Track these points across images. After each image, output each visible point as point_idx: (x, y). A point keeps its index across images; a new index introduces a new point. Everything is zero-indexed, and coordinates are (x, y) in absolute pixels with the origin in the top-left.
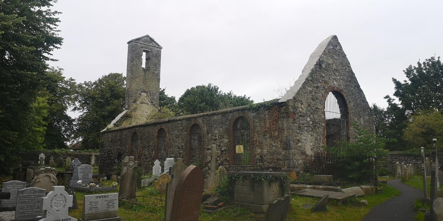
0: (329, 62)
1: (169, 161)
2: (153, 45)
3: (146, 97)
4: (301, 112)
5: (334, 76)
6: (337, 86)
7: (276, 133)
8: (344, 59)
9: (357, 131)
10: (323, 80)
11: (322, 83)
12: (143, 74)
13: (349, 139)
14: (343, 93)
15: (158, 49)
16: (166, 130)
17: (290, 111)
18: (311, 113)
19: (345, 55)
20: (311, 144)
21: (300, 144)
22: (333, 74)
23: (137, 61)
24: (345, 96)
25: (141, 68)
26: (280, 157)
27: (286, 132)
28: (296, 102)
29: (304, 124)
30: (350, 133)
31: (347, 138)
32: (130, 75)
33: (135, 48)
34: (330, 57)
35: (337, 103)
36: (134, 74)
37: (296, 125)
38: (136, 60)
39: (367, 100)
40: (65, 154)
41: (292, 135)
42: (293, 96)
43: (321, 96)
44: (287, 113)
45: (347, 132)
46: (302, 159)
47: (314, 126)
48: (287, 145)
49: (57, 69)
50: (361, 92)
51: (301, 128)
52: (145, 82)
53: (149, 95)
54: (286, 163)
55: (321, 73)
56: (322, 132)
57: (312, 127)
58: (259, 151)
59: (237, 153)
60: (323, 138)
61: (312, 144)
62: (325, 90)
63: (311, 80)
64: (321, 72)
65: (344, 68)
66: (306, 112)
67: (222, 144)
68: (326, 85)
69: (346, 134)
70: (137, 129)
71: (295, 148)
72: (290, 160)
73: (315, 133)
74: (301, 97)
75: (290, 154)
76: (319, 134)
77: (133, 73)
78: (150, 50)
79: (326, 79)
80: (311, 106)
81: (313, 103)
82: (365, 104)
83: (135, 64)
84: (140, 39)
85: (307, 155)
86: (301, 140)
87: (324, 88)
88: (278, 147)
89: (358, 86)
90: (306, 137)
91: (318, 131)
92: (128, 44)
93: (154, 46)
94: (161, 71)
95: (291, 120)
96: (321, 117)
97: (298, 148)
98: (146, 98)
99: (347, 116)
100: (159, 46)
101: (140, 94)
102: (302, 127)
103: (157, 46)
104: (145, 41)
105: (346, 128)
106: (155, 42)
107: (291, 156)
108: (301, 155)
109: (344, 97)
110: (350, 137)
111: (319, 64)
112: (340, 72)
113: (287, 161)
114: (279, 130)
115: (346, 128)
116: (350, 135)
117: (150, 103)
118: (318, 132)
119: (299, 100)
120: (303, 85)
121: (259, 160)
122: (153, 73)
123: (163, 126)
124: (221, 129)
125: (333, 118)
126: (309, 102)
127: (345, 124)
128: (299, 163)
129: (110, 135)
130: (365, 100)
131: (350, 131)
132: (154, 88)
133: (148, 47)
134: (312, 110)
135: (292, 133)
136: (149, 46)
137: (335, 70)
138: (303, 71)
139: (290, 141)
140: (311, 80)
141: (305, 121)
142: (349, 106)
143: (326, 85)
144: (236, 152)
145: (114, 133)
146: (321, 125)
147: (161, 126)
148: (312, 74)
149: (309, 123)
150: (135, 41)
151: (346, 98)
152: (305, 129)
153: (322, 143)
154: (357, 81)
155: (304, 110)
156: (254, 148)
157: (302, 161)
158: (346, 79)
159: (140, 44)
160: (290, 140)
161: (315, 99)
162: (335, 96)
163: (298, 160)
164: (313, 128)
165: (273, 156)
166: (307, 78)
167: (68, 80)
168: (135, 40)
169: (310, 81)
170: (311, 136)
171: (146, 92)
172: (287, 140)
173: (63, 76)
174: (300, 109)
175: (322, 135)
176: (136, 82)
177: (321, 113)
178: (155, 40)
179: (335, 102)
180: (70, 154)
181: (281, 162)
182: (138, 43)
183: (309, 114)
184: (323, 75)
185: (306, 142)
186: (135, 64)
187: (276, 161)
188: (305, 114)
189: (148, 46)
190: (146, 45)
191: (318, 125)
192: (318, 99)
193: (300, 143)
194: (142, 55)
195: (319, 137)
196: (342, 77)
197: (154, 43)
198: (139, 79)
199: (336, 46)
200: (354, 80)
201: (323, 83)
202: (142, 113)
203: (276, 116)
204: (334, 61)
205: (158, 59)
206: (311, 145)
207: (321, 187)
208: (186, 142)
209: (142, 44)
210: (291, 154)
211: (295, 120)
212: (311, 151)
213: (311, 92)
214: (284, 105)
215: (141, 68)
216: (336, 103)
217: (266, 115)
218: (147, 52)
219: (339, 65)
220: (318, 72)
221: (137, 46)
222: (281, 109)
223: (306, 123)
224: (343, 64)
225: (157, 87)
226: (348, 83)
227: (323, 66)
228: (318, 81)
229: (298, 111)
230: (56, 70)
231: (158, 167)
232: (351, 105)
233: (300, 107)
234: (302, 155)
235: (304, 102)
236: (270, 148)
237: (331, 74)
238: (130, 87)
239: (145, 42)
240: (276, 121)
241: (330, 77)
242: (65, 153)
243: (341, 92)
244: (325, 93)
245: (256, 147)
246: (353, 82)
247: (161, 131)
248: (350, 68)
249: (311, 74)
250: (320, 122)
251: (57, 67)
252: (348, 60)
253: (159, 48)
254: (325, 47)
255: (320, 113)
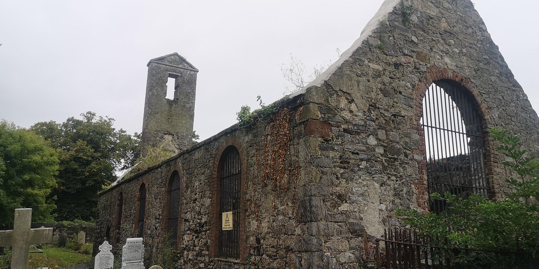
0: (428, 11)
1: (131, 244)
2: (184, 67)
3: (172, 141)
4: (347, 122)
5: (443, 45)
6: (453, 68)
7: (285, 180)
8: (470, 11)
9: (510, 160)
10: (414, 52)
11: (409, 56)
12: (167, 108)
13: (495, 196)
14: (469, 86)
17: (315, 117)
18: (380, 126)
19: (471, 3)
20: (380, 208)
21: (344, 207)
22: (442, 41)
23: (159, 89)
24: (475, 92)
25: (164, 100)
26: (292, 243)
27: (303, 172)
28: (331, 95)
29: (358, 154)
30: (495, 182)
31: (488, 192)
32: (148, 109)
33: (156, 72)
34: (432, 3)
35: (455, 109)
36: (154, 108)
37: (331, 154)
38: (157, 88)
39: (534, 108)
40: (78, 227)
41: (318, 181)
42: (323, 79)
43: (410, 86)
44: (306, 122)
45: (488, 180)
46: (351, 248)
47: (390, 158)
48: (305, 209)
49: (106, 119)
50: (518, 89)
51: (348, 163)
52: (170, 120)
53: (176, 138)
54: (303, 262)
55: (406, 34)
56: (414, 176)
57: (384, 161)
58: (254, 224)
59: (223, 230)
60: (419, 192)
61: (383, 207)
62: (419, 75)
63: (379, 48)
64: (407, 32)
65: (470, 30)
66: (365, 122)
68: (422, 63)
69: (485, 185)
71: (329, 217)
72: (312, 252)
73: (393, 178)
74: (349, 83)
75: (312, 235)
76: (404, 180)
77: (151, 107)
78: (179, 74)
79: (424, 48)
80: (379, 108)
81: (385, 101)
82: (530, 117)
83: (156, 93)
84: (163, 58)
85: (369, 238)
86: (350, 194)
87: (418, 69)
88: (288, 214)
89: (509, 75)
90: (366, 188)
91: (401, 174)
92: (148, 67)
93: (185, 68)
94: (195, 104)
95: (316, 141)
96: (409, 137)
97: (340, 218)
98: (171, 143)
99: (484, 142)
100: (194, 68)
101: (162, 138)
102: (352, 161)
103: (190, 68)
104: (172, 62)
105: (483, 171)
106: (188, 63)
107: (315, 241)
108: (347, 238)
109: (473, 96)
110: (497, 190)
112: (459, 37)
113: (305, 256)
114: (290, 171)
115: (483, 171)
116: (496, 186)
118: (401, 176)
119: (340, 90)
120: (353, 55)
121: (254, 248)
122: (183, 106)
125: (456, 155)
126: (372, 99)
127: (482, 160)
128: (342, 260)
130: (529, 107)
131: (495, 177)
132: (183, 128)
133: (176, 69)
134: (382, 118)
135: (319, 176)
136: (179, 69)
137: (445, 31)
139: (313, 198)
140: (379, 48)
141: (360, 145)
142: (487, 117)
143: (422, 63)
144: (223, 226)
146: (412, 159)
148: (381, 32)
149: (374, 151)
150: (155, 61)
151: (479, 99)
152: (361, 167)
153: (416, 204)
154: (505, 62)
155: (356, 116)
156: (246, 217)
157: (351, 255)
158: (475, 55)
159: (164, 66)
160: (312, 196)
161: (392, 91)
162: (446, 91)
163: (340, 252)
164: (386, 164)
165: (279, 239)
166: (367, 41)
167: (118, 132)
168: (156, 60)
169: (375, 48)
170: (381, 186)
171: (171, 134)
172: (305, 195)
173: (112, 127)
174: (346, 115)
175: (415, 184)
176: (156, 119)
177: (408, 126)
178: (188, 60)
179: (451, 107)
180: (85, 228)
181: (293, 256)
182: (161, 64)
183: (374, 129)
184: (414, 39)
185: (365, 202)
186: (156, 93)
187: (282, 252)
188: (361, 128)
189: (176, 68)
190: (174, 68)
191: (402, 157)
192: (400, 93)
193: (346, 205)
194: (166, 81)
195: (405, 190)
196: (464, 50)
197: (186, 64)
198: (161, 115)
200: (496, 61)
201: (415, 57)
203: (285, 135)
204: (442, 11)
205: (192, 87)
206: (381, 210)
209: (166, 65)
210: (314, 234)
211: (330, 142)
213: (378, 75)
214: (302, 104)
215: (164, 100)
216: (453, 108)
217: (268, 135)
219: (457, 22)
220: (397, 31)
221: (160, 69)
222: (295, 116)
223: (364, 151)
224: (466, 23)
225: (188, 126)
226: (481, 64)
227: (414, 18)
228: (400, 52)
229: (338, 118)
230: (106, 121)
231: (106, 255)
233: (344, 110)
234: (351, 238)
235: (356, 95)
236: (274, 217)
237: (434, 39)
238: (146, 128)
239: (172, 63)
240: (285, 146)
241: (434, 47)
242: (77, 226)
243: (464, 83)
244: (420, 81)
245: (249, 215)
246: (494, 63)
248: (486, 33)
249: (377, 32)
250: (408, 152)
251: (106, 116)
252: (478, 16)
253: (194, 71)
255: (406, 128)
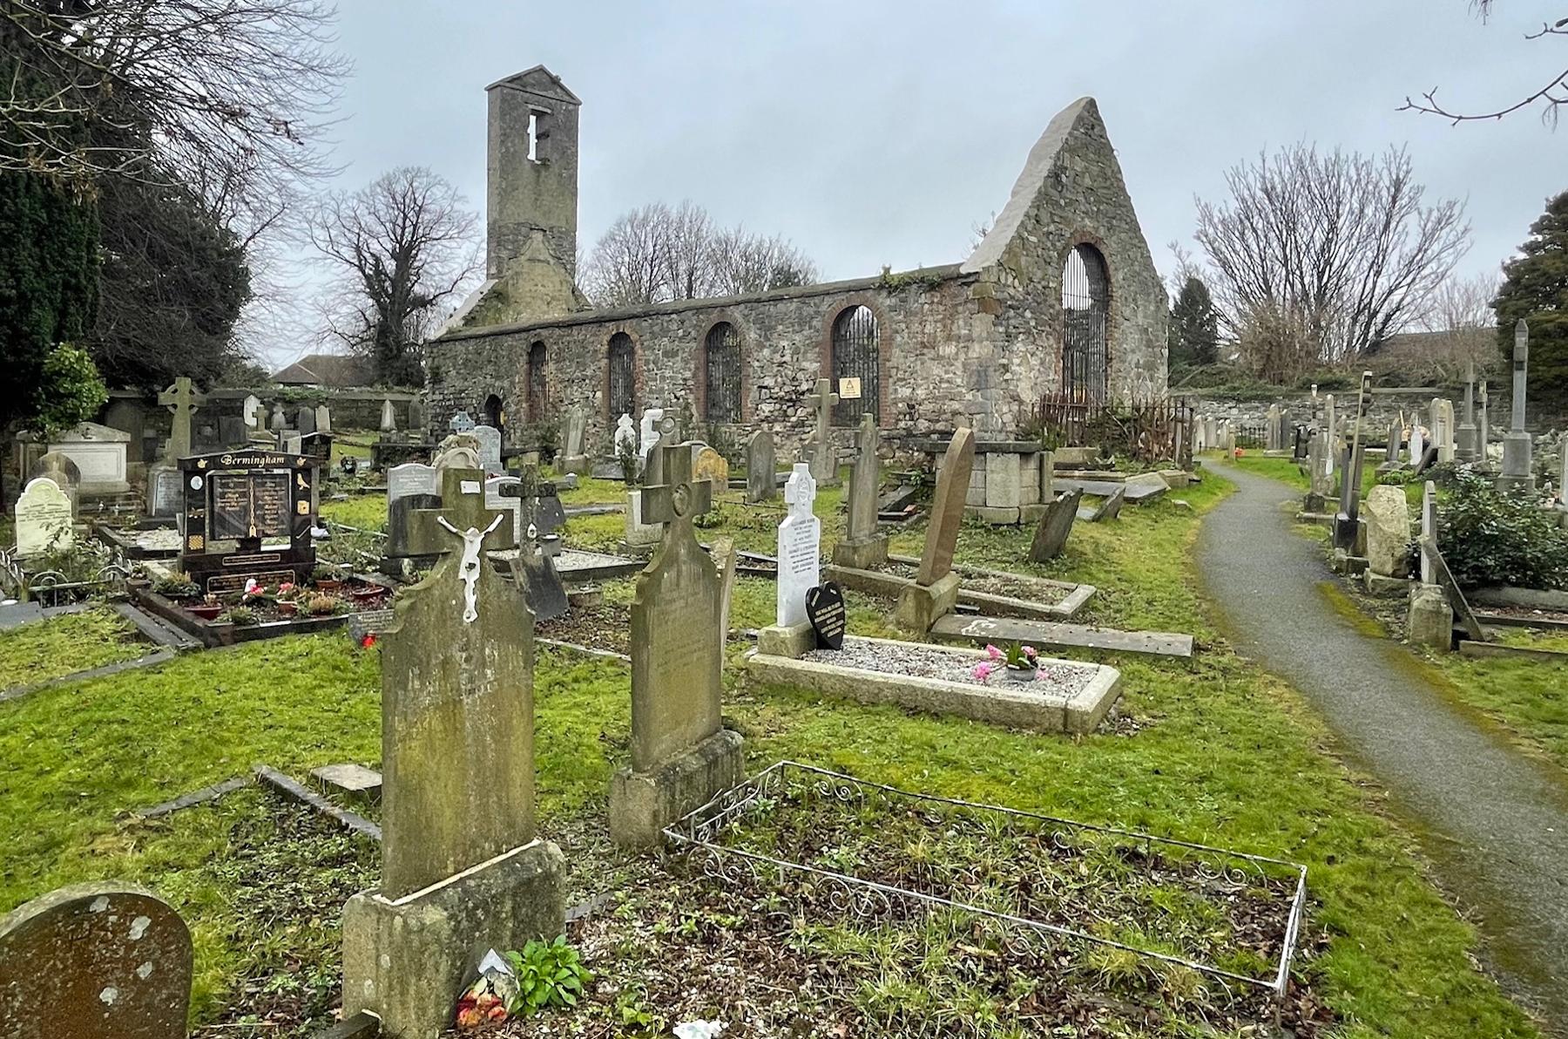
4: (1012, 298)
15: (571, 107)
16: (634, 337)
65: (1108, 183)
67: (800, 375)
70: (544, 333)
106: (562, 88)
111: (1055, 176)
117: (552, 262)
123: (627, 327)
124: (797, 338)
129: (459, 347)
138: (1014, 194)
142: (1113, 280)
145: (472, 342)
147: (618, 328)
151: (1108, 261)
197: (559, 90)
199: (1093, 128)
202: (534, 289)
207: (1077, 473)
208: (697, 368)
212: (1029, 392)
218: (540, 115)
232: (1117, 277)
243: (1097, 246)
247: (619, 340)
254: (1068, 130)
